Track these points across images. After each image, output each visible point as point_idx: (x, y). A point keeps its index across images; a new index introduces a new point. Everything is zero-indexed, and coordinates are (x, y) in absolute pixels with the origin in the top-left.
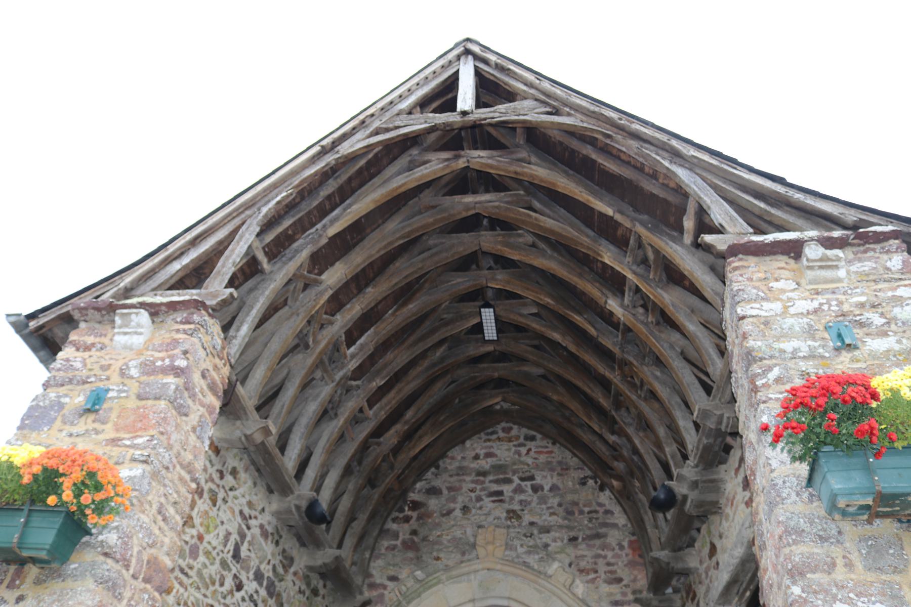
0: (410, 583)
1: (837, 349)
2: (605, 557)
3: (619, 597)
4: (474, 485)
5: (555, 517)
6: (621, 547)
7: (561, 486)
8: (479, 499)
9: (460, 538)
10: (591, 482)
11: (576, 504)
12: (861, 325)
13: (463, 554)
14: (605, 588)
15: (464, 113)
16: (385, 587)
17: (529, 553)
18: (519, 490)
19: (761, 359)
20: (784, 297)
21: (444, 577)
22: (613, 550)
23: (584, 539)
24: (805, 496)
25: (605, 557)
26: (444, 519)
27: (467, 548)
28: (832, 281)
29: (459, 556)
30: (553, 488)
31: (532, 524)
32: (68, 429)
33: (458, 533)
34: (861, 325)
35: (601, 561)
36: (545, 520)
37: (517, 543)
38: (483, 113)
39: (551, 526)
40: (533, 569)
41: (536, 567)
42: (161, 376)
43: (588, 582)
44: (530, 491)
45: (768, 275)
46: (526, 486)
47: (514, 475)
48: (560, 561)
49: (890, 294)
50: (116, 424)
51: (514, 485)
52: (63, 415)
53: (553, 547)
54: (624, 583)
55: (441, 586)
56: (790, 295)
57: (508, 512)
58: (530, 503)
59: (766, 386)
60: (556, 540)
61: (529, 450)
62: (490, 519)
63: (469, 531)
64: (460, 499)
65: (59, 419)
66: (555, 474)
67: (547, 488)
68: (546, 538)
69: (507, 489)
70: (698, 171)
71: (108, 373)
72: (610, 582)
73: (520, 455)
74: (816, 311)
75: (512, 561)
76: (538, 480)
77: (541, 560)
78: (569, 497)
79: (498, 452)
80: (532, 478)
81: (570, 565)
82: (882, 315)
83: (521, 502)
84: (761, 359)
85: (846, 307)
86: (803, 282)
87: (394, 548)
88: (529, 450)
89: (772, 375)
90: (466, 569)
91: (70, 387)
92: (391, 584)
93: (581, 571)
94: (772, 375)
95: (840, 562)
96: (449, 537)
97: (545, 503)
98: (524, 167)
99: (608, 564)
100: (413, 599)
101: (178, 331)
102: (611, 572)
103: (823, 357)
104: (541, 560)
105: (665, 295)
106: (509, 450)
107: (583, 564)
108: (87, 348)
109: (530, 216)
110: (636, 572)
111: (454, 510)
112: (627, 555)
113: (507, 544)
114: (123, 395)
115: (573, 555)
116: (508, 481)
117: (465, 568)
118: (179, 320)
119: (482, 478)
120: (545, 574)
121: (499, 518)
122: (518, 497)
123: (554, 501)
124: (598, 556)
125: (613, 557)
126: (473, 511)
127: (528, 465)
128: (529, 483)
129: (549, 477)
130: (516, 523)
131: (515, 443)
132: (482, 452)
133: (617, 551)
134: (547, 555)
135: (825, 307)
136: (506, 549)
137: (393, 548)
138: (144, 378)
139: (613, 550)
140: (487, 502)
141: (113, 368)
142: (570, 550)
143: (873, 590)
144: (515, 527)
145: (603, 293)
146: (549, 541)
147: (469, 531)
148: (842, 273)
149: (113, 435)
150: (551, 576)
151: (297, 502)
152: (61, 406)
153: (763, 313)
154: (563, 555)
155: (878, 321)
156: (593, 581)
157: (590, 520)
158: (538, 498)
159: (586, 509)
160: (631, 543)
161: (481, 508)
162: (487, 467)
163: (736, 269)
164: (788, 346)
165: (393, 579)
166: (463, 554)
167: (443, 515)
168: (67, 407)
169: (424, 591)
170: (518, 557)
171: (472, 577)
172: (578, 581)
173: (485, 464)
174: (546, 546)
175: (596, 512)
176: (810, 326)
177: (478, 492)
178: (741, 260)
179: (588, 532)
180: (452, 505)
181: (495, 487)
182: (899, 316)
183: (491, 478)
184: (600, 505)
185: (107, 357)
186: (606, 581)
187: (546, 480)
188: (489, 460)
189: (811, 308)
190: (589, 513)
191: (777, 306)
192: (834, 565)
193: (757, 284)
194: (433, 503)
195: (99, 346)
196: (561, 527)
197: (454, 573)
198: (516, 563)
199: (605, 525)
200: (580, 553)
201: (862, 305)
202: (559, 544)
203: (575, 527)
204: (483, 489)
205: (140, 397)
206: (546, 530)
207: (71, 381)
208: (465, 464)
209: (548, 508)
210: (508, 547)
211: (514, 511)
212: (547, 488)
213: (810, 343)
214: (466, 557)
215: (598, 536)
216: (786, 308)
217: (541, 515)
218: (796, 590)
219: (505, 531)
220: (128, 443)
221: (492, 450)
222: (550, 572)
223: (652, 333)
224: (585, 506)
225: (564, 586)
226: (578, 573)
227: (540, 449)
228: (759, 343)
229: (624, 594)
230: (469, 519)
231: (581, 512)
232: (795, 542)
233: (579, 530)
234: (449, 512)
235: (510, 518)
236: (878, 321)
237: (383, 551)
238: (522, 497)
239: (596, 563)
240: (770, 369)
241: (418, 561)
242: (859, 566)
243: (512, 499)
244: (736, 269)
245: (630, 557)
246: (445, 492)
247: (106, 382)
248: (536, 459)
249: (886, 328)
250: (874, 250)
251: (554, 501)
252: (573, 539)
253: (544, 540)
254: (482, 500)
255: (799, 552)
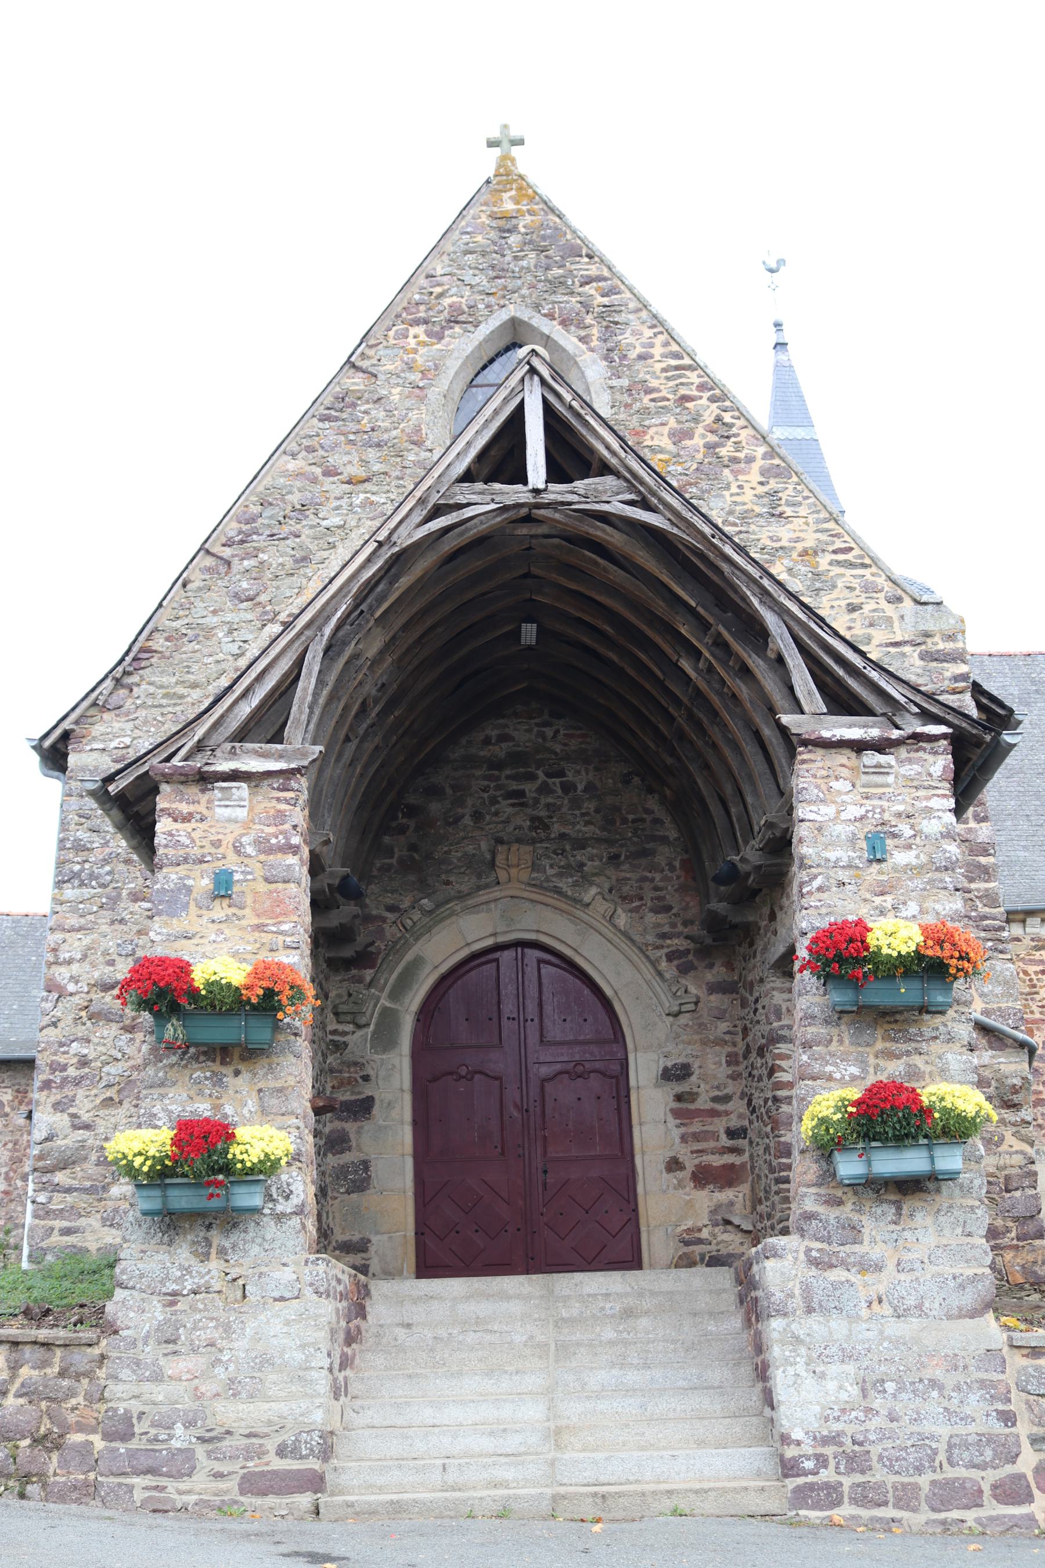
0: (416, 915)
1: (870, 861)
2: (652, 880)
3: (667, 929)
4: (486, 783)
5: (592, 827)
6: (672, 868)
7: (598, 784)
8: (494, 801)
9: (474, 855)
10: (636, 780)
11: (617, 809)
12: (894, 836)
13: (479, 876)
14: (651, 918)
15: (536, 491)
16: (384, 920)
17: (560, 875)
18: (545, 789)
19: (810, 867)
20: (839, 800)
21: (458, 908)
22: (662, 871)
23: (627, 857)
24: (821, 992)
25: (652, 880)
26: (450, 830)
27: (484, 869)
28: (882, 786)
29: (474, 879)
30: (589, 787)
31: (563, 836)
32: (207, 915)
33: (470, 849)
34: (894, 836)
35: (647, 885)
36: (580, 831)
37: (546, 862)
38: (558, 492)
39: (587, 839)
40: (566, 896)
41: (570, 893)
42: (280, 855)
43: (631, 911)
44: (559, 791)
45: (831, 772)
46: (554, 784)
47: (538, 769)
48: (598, 886)
49: (924, 804)
50: (254, 910)
51: (539, 782)
52: (195, 900)
53: (589, 867)
54: (674, 911)
55: (454, 918)
56: (845, 798)
57: (534, 819)
58: (560, 808)
59: (810, 893)
60: (591, 858)
61: (557, 732)
62: (510, 828)
63: (484, 845)
64: (470, 802)
65: (192, 904)
66: (591, 767)
67: (580, 787)
68: (580, 856)
69: (529, 788)
70: (786, 618)
71: (221, 850)
72: (655, 911)
73: (544, 738)
74: (862, 818)
75: (541, 887)
76: (570, 777)
77: (575, 884)
78: (609, 800)
79: (515, 734)
80: (561, 774)
81: (610, 891)
82: (912, 827)
83: (548, 806)
84: (810, 867)
85: (887, 816)
86: (858, 784)
87: (387, 868)
88: (557, 732)
89: (816, 884)
90: (485, 898)
91: (187, 866)
92: (391, 916)
93: (624, 898)
94: (816, 884)
95: (835, 1038)
96: (459, 854)
97: (579, 808)
98: (598, 528)
99: (656, 889)
100: (422, 935)
101: (278, 799)
102: (658, 898)
103: (857, 868)
104: (575, 884)
105: (744, 688)
106: (529, 731)
107: (626, 889)
108: (187, 818)
109: (596, 563)
110: (688, 899)
111: (463, 816)
112: (678, 877)
113: (533, 863)
114: (249, 877)
115: (614, 878)
116: (532, 777)
117: (483, 896)
118: (275, 786)
119: (496, 773)
120: (581, 901)
121: (520, 828)
122: (544, 800)
123: (590, 806)
124: (644, 879)
125: (661, 880)
126: (488, 817)
127: (555, 753)
128: (557, 780)
129: (583, 772)
130: (543, 835)
131: (537, 721)
132: (494, 733)
133: (667, 872)
134: (582, 877)
135: (870, 815)
136: (533, 870)
137: (386, 869)
138: (262, 857)
139: (662, 871)
140: (506, 807)
141: (224, 843)
142: (611, 872)
143: (851, 1058)
144: (541, 841)
145: (676, 651)
146: (584, 860)
147: (484, 845)
148: (890, 779)
149: (256, 921)
150: (588, 905)
151: (331, 882)
152: (189, 890)
153: (819, 818)
154: (603, 878)
155: (908, 832)
156: (636, 910)
157: (635, 831)
158: (570, 800)
159: (631, 817)
160: (683, 862)
161: (496, 814)
162: (502, 755)
163: (803, 762)
164: (832, 855)
165: (391, 909)
166: (479, 876)
167: (450, 824)
168: (195, 890)
169: (435, 925)
170: (547, 880)
171: (493, 905)
172: (619, 911)
173: (500, 751)
174: (582, 865)
175: (643, 820)
176: (854, 834)
177: (491, 792)
178: (810, 751)
179: (633, 849)
180: (460, 811)
181: (514, 786)
182: (925, 830)
183: (508, 772)
184: (648, 811)
185: (213, 830)
186: (652, 910)
187: (580, 777)
188: (504, 745)
189: (858, 816)
190: (634, 821)
191: (830, 810)
192: (831, 1041)
193: (819, 781)
194: (435, 807)
195: (198, 816)
196: (599, 840)
197: (470, 902)
198: (546, 889)
199: (653, 838)
200: (623, 874)
201: (899, 815)
202: (597, 863)
203: (617, 841)
204: (498, 788)
205: (267, 880)
206: (580, 844)
207: (186, 860)
208: (473, 751)
209: (583, 815)
210: (535, 867)
211: (539, 819)
212: (580, 787)
213: (850, 853)
214: (484, 881)
215: (644, 853)
216: (839, 812)
217: (574, 824)
218: (805, 1058)
219: (530, 848)
220: (274, 929)
221: (507, 730)
222: (587, 899)
223: (726, 707)
224: (628, 813)
225: (604, 917)
226: (619, 901)
227: (571, 732)
228: (811, 851)
229: (673, 925)
230: (482, 829)
231: (624, 821)
232: (810, 1025)
233: (622, 846)
234: (458, 819)
235: (536, 828)
236: (908, 832)
237: (375, 873)
238: (550, 800)
239: (641, 888)
240: (815, 877)
241: (424, 887)
242: (847, 1042)
243: (536, 801)
244: (803, 762)
245: (682, 879)
246: (449, 791)
247: (223, 862)
248: (565, 745)
249: (912, 841)
250: (924, 750)
251: (590, 806)
252: (614, 858)
253: (578, 858)
254: (498, 802)
255: (813, 1031)
